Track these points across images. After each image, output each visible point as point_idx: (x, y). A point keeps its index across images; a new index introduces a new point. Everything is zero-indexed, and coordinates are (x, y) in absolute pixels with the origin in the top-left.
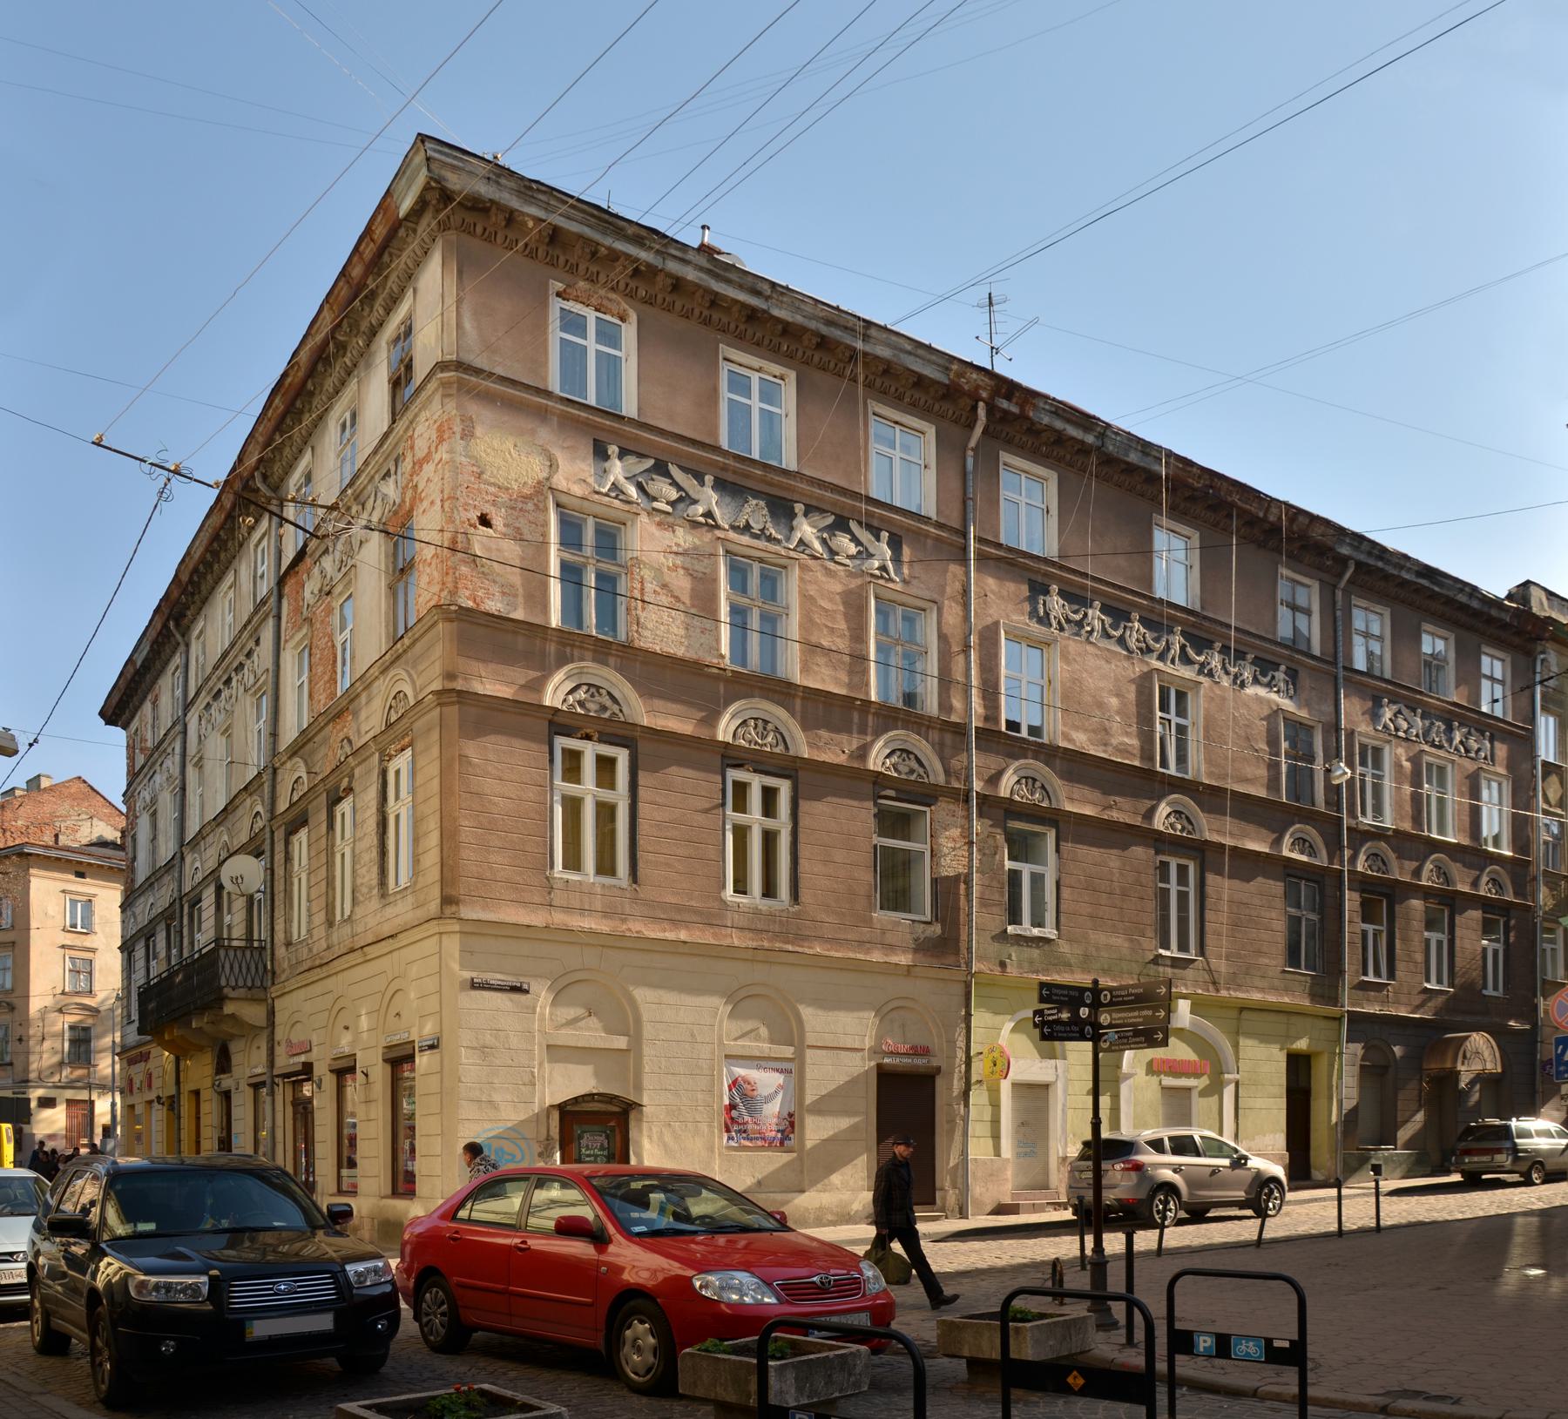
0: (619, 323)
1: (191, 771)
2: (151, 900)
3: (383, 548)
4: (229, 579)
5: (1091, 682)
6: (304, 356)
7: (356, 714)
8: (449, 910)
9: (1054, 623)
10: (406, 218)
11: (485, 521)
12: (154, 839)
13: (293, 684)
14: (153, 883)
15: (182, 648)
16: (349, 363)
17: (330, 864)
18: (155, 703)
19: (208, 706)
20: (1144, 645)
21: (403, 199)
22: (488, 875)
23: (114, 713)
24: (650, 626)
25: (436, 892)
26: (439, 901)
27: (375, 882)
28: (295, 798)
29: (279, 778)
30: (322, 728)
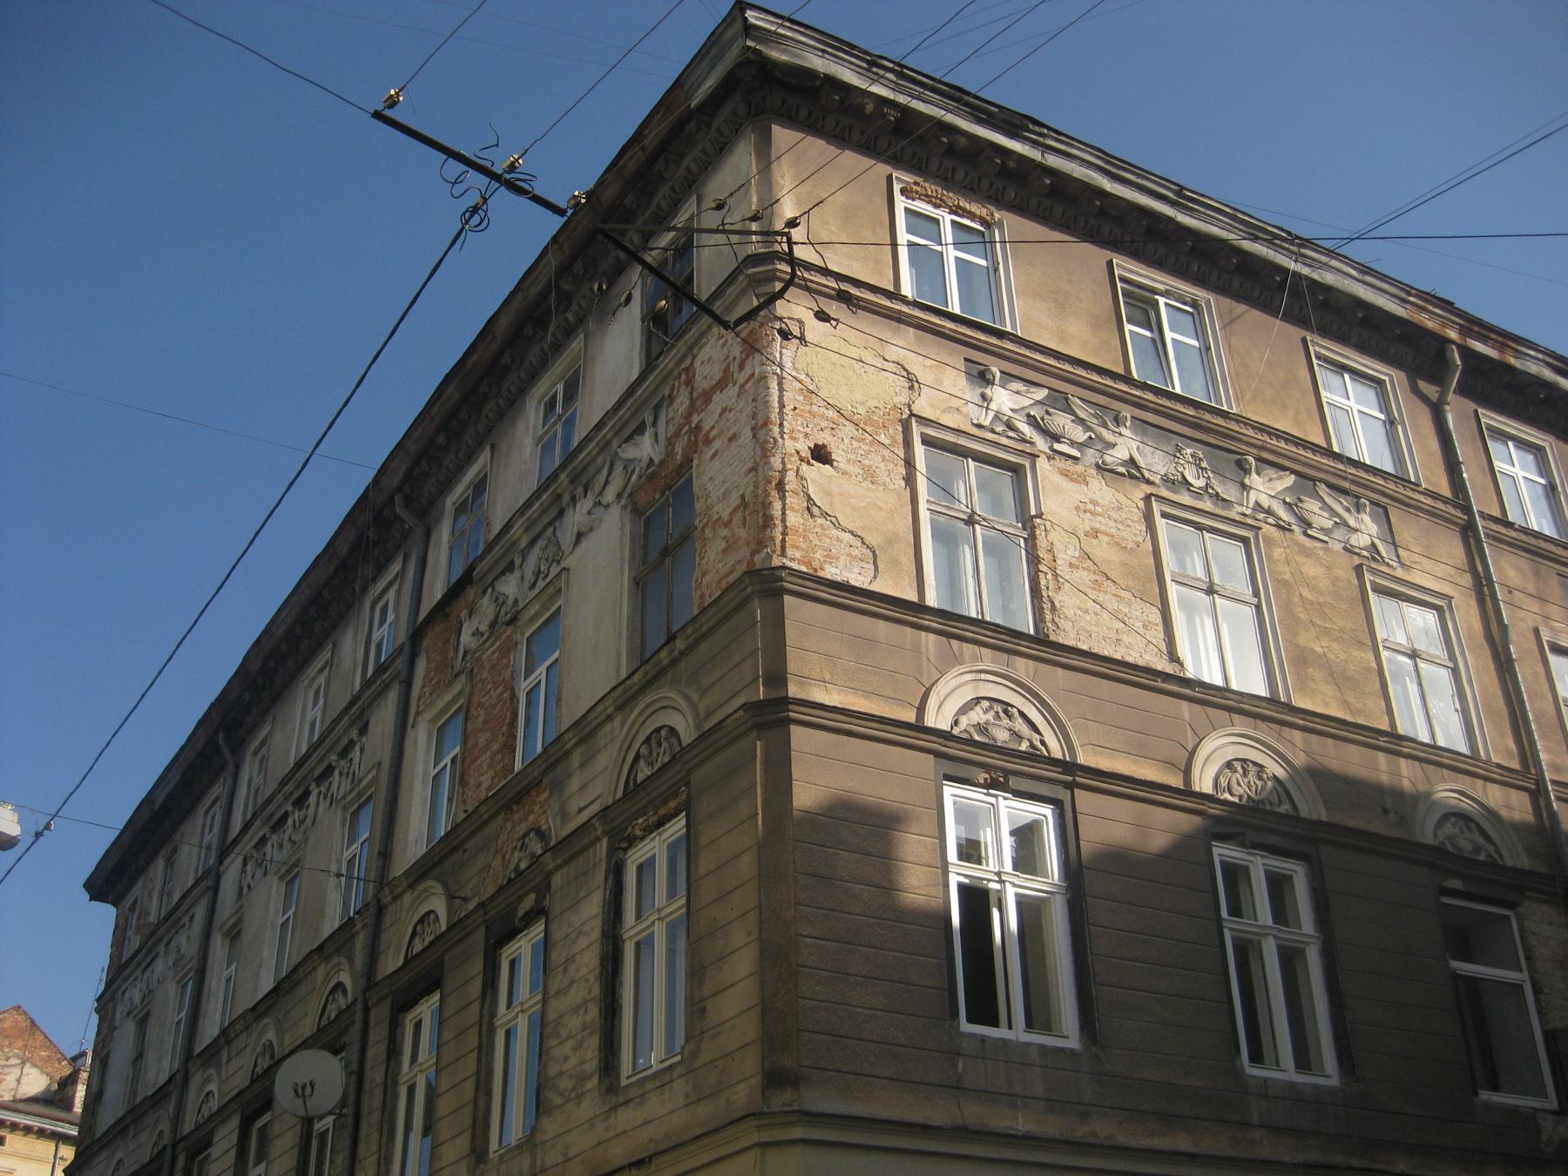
1: (219, 946)
2: (119, 1155)
3: (627, 529)
4: (325, 655)
6: (504, 322)
7: (558, 787)
8: (781, 1099)
11: (820, 454)
12: (140, 1056)
13: (425, 773)
14: (126, 1128)
15: (231, 769)
17: (485, 1050)
18: (170, 862)
19: (263, 841)
24: (1070, 613)
25: (749, 1066)
26: (756, 1081)
27: (592, 1065)
28: (418, 947)
29: (387, 921)
30: (485, 824)
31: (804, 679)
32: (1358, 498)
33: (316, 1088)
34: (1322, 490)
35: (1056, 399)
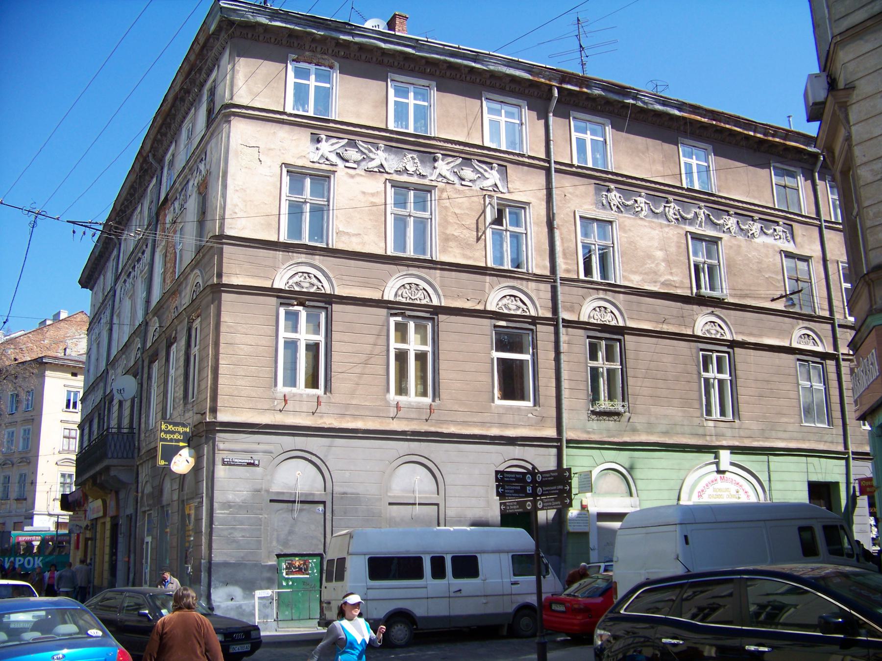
0: (329, 70)
5: (643, 243)
7: (180, 293)
9: (614, 208)
10: (213, 34)
14: (94, 387)
15: (118, 246)
16: (191, 100)
19: (125, 281)
20: (678, 217)
21: (211, 26)
22: (235, 393)
23: (86, 282)
27: (182, 396)
31: (229, 275)
32: (492, 164)
33: (125, 390)
34: (475, 163)
35: (351, 143)
